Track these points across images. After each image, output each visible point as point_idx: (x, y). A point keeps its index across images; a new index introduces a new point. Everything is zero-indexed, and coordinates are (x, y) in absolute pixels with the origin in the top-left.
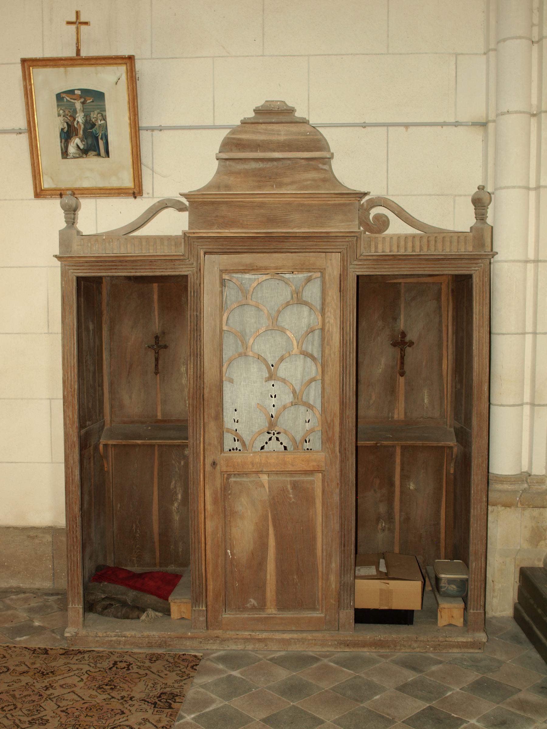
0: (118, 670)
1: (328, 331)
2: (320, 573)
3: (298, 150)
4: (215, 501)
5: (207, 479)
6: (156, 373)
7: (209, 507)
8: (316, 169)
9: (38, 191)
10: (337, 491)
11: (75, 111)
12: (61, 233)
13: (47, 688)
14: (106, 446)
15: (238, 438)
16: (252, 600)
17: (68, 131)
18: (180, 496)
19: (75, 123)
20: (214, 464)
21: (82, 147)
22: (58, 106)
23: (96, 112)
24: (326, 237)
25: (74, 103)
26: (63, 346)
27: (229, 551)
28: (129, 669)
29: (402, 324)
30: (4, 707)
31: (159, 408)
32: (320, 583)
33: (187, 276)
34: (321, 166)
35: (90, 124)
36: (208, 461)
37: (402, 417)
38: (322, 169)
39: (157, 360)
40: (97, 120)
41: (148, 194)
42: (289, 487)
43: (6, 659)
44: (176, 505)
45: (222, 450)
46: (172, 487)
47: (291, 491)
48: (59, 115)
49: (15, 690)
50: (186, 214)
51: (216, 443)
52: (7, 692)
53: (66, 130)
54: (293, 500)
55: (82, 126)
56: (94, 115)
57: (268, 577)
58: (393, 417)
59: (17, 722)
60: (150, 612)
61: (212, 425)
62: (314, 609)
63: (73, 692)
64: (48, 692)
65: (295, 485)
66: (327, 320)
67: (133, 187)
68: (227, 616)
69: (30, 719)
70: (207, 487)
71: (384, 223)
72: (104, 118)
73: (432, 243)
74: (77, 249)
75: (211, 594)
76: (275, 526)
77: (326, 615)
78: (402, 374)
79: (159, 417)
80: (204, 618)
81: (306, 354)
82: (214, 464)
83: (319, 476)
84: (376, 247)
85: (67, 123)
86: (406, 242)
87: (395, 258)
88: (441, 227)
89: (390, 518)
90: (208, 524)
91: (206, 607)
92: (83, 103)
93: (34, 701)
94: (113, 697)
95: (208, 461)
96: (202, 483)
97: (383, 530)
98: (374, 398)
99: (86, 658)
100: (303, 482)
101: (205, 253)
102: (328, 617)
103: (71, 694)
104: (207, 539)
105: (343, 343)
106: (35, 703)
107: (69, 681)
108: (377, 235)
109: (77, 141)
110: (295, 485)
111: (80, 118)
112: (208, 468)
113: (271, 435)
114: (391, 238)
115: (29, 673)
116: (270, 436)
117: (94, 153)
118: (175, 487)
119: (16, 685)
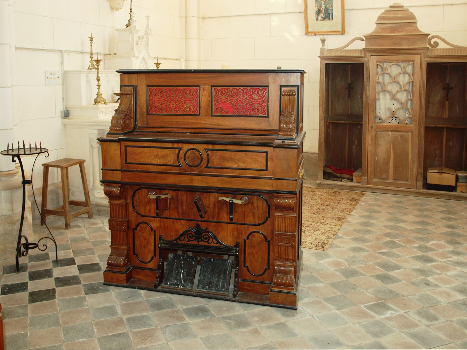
1: (415, 82)
2: (410, 167)
3: (406, 19)
4: (372, 140)
5: (369, 132)
6: (349, 97)
7: (369, 142)
8: (412, 26)
9: (307, 32)
10: (417, 139)
11: (321, 5)
12: (321, 49)
14: (329, 123)
15: (380, 119)
16: (384, 176)
17: (318, 12)
18: (356, 143)
19: (321, 9)
20: (372, 127)
21: (323, 17)
22: (315, 3)
23: (329, 5)
24: (416, 49)
25: (321, 2)
26: (320, 86)
27: (376, 158)
29: (448, 81)
31: (350, 110)
32: (410, 172)
33: (364, 63)
34: (414, 25)
35: (327, 9)
36: (370, 126)
37: (447, 117)
38: (414, 26)
39: (349, 93)
40: (329, 8)
41: (347, 33)
42: (399, 136)
44: (354, 146)
45: (375, 123)
46: (353, 139)
47: (400, 138)
48: (316, 6)
50: (364, 42)
51: (373, 120)
53: (318, 11)
54: (400, 141)
55: (324, 10)
56: (328, 6)
57: (390, 168)
58: (443, 117)
60: (346, 179)
61: (371, 114)
62: (407, 181)
65: (401, 136)
66: (415, 79)
67: (342, 31)
68: (375, 180)
70: (369, 134)
71: (436, 44)
72: (332, 7)
73: (457, 51)
74: (326, 54)
75: (369, 172)
76: (393, 150)
77: (411, 183)
78: (447, 100)
79: (349, 113)
80: (366, 181)
81: (406, 90)
82: (372, 127)
83: (410, 134)
84: (435, 53)
85: (318, 9)
86: (446, 51)
87: (441, 57)
88: (460, 45)
89: (441, 156)
90: (369, 147)
91: (367, 177)
92: (324, 2)
95: (370, 126)
96: (367, 134)
97: (438, 160)
98: (435, 109)
100: (404, 135)
101: (371, 55)
102: (412, 184)
104: (369, 152)
105: (421, 86)
108: (435, 48)
109: (322, 15)
110: (401, 136)
111: (323, 7)
112: (370, 128)
113: (393, 118)
114: (440, 49)
116: (392, 118)
117: (328, 19)
118: (355, 140)
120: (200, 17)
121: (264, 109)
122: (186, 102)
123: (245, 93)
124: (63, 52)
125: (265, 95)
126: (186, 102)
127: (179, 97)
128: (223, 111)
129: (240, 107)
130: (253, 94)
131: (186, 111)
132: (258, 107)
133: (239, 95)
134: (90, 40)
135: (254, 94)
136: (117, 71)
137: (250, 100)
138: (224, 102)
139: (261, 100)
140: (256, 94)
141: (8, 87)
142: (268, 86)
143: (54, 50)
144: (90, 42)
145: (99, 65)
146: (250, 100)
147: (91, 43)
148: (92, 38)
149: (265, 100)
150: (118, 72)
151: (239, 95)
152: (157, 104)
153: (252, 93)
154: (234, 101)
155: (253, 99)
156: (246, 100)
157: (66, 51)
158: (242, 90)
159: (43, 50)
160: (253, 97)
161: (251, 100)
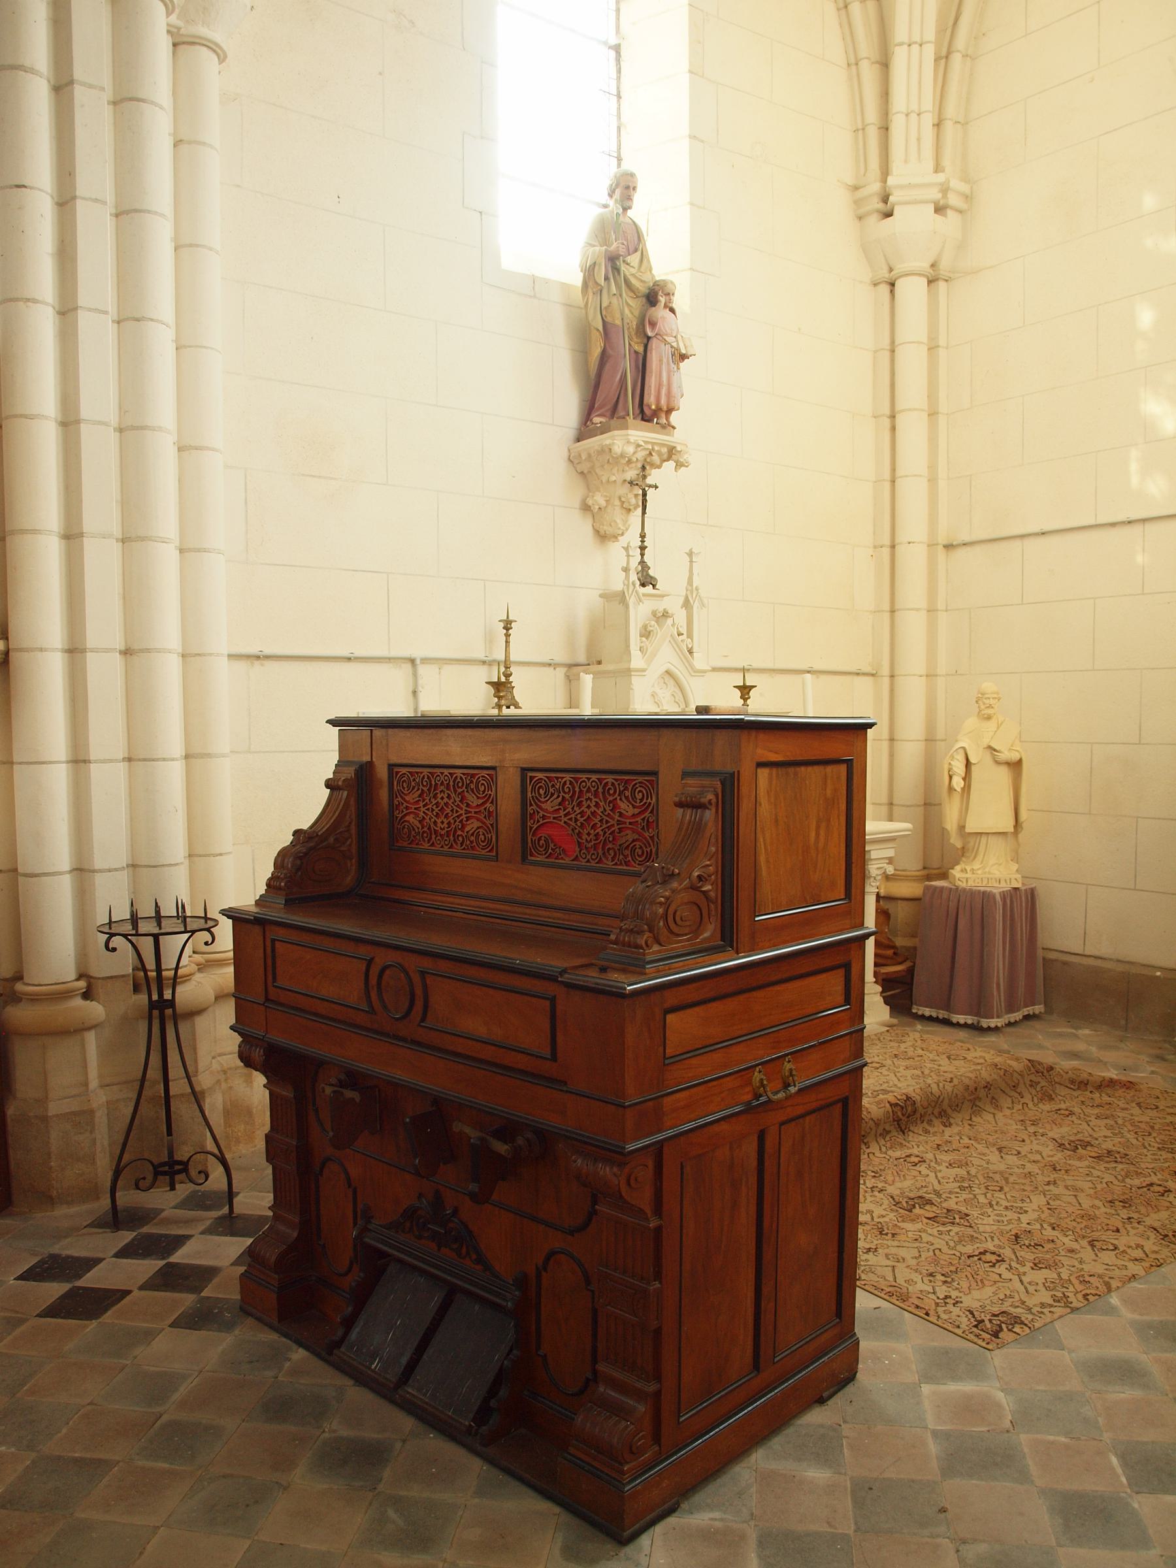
0: (1148, 1192)
13: (1048, 1183)
28: (1163, 1195)
30: (1088, 1295)
43: (1119, 1234)
49: (1113, 1278)
52: (1100, 1276)
59: (994, 1203)
63: (1075, 1196)
64: (1047, 1188)
69: (1008, 1204)
93: (1024, 1190)
94: (1118, 1215)
99: (1118, 1169)
103: (992, 1116)
106: (1025, 1193)
107: (1080, 1184)
115: (1143, 1264)
119: (1117, 1272)
120: (937, 544)
121: (649, 850)
122: (623, 826)
123: (601, 795)
124: (418, 662)
125: (650, 803)
126: (623, 826)
127: (606, 811)
128: (550, 851)
129: (589, 839)
130: (621, 799)
131: (621, 857)
132: (634, 841)
133: (587, 800)
134: (504, 628)
135: (623, 799)
136: (329, 722)
137: (613, 819)
138: (551, 820)
139: (639, 819)
140: (627, 798)
141: (173, 760)
142: (655, 773)
143: (389, 659)
144: (505, 631)
145: (749, 698)
146: (613, 819)
147: (507, 635)
148: (511, 622)
149: (651, 820)
150: (334, 722)
151: (587, 800)
152: (410, 818)
153: (619, 795)
154: (576, 820)
155: (621, 815)
156: (604, 817)
157: (425, 660)
158: (593, 784)
159: (349, 659)
160: (619, 808)
161: (617, 817)
